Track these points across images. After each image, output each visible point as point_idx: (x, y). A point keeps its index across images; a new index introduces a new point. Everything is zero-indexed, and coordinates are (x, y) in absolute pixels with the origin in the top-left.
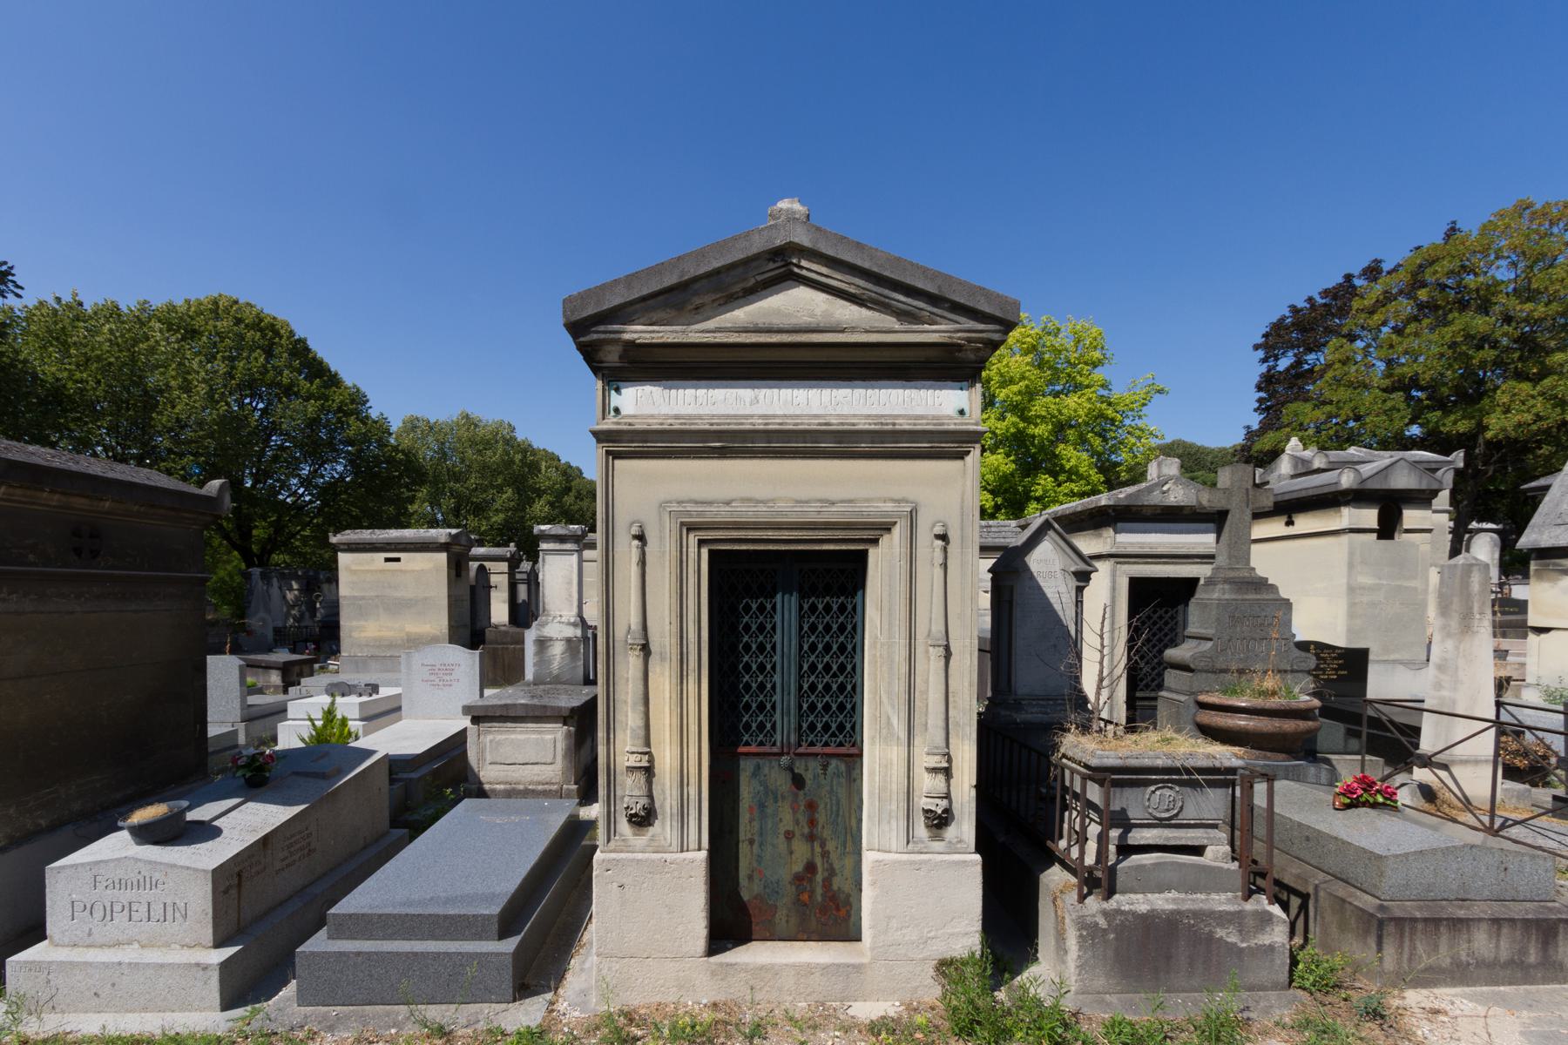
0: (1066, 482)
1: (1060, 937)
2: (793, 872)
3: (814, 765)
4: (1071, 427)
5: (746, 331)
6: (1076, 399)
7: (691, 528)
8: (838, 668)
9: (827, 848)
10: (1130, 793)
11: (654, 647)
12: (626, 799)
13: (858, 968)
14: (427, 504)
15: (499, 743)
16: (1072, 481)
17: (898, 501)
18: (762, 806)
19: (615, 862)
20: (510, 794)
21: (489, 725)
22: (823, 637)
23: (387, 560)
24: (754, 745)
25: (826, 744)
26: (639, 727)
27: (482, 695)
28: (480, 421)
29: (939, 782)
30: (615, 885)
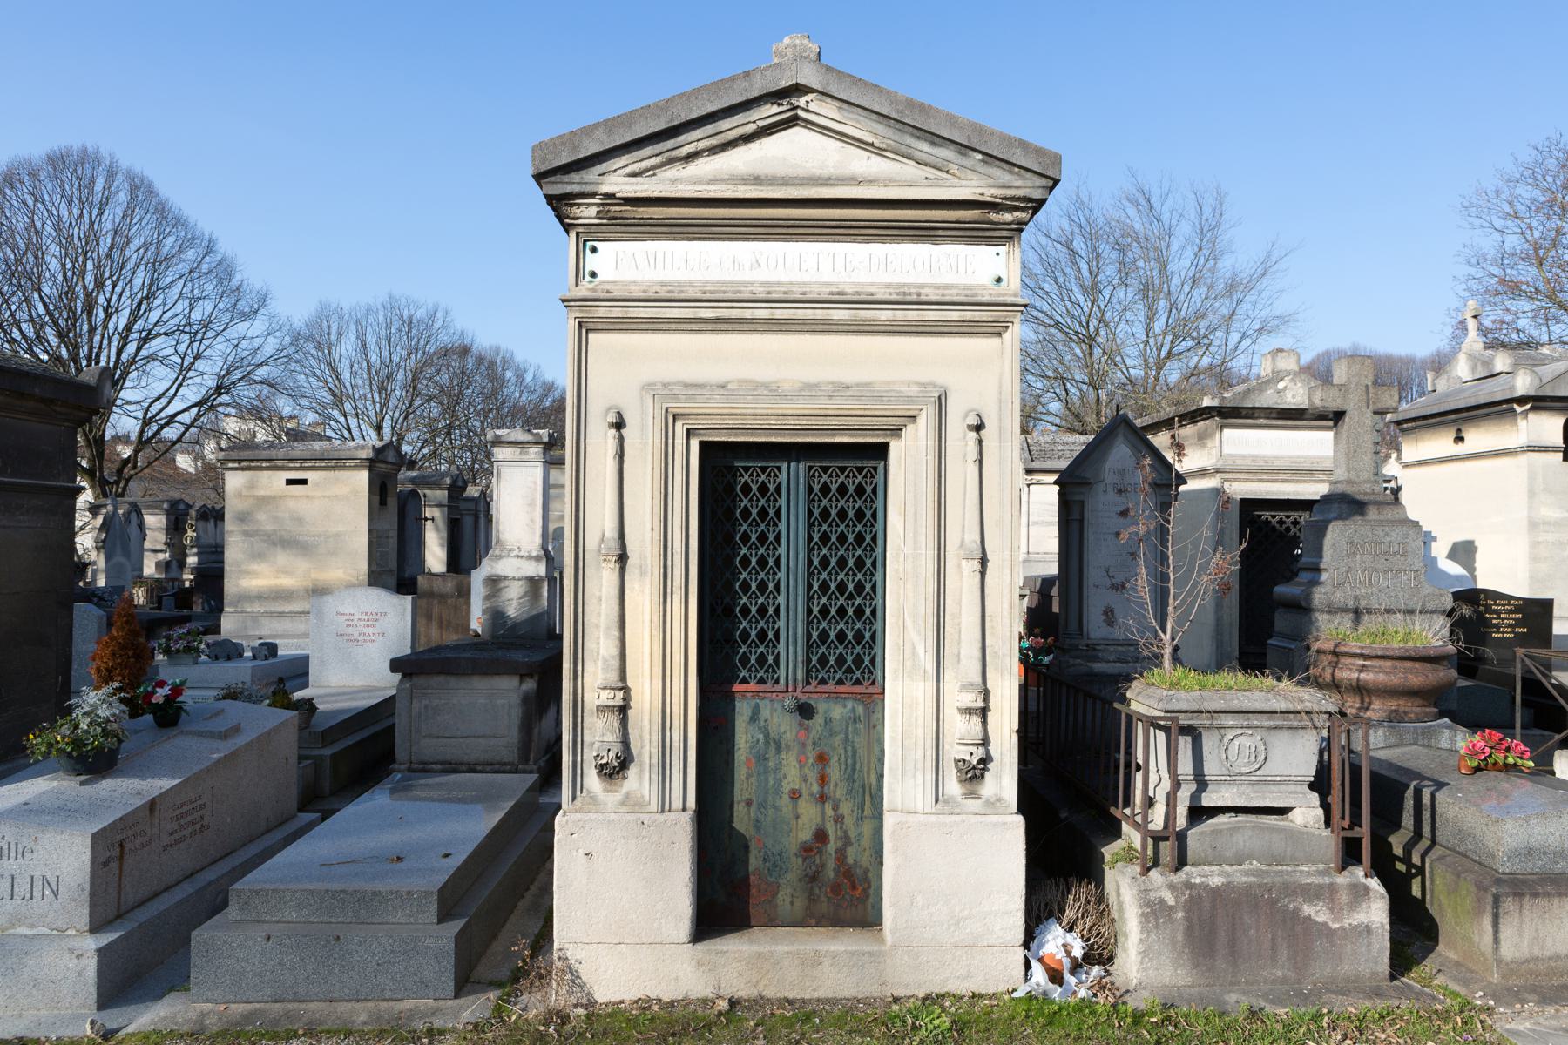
2: (800, 841)
9: (840, 812)
18: (762, 758)
19: (581, 824)
23: (290, 482)
25: (840, 682)
26: (613, 657)
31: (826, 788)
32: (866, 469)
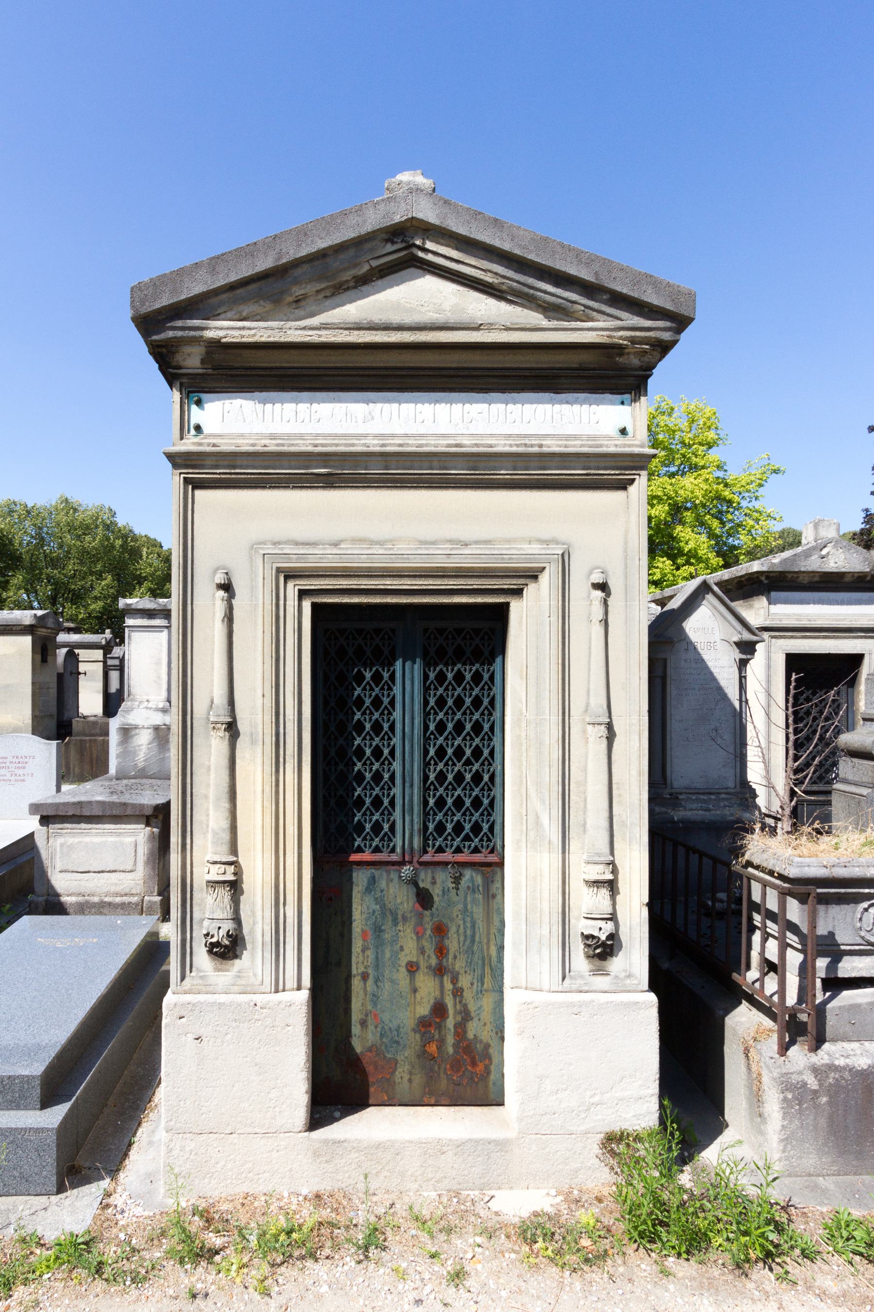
0: (684, 565)
1: (756, 1098)
2: (418, 1015)
3: (443, 877)
4: (687, 509)
5: (359, 327)
6: (692, 480)
7: (290, 575)
8: (473, 753)
9: (460, 985)
10: (835, 910)
11: (242, 726)
12: (206, 923)
13: (502, 1145)
14: (22, 591)
15: (71, 847)
16: (692, 564)
17: (547, 542)
18: (378, 930)
20: (83, 908)
21: (60, 826)
22: (454, 713)
24: (368, 851)
25: (458, 850)
27: (58, 790)
28: (80, 505)
29: (601, 900)
30: (191, 1037)
31: (444, 960)
32: (465, 632)
